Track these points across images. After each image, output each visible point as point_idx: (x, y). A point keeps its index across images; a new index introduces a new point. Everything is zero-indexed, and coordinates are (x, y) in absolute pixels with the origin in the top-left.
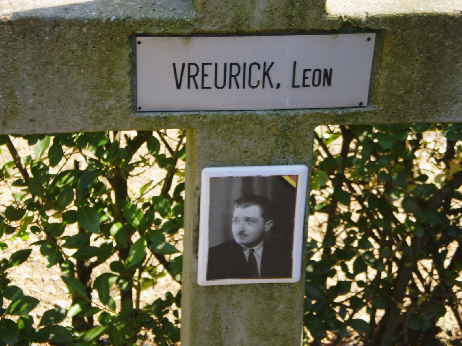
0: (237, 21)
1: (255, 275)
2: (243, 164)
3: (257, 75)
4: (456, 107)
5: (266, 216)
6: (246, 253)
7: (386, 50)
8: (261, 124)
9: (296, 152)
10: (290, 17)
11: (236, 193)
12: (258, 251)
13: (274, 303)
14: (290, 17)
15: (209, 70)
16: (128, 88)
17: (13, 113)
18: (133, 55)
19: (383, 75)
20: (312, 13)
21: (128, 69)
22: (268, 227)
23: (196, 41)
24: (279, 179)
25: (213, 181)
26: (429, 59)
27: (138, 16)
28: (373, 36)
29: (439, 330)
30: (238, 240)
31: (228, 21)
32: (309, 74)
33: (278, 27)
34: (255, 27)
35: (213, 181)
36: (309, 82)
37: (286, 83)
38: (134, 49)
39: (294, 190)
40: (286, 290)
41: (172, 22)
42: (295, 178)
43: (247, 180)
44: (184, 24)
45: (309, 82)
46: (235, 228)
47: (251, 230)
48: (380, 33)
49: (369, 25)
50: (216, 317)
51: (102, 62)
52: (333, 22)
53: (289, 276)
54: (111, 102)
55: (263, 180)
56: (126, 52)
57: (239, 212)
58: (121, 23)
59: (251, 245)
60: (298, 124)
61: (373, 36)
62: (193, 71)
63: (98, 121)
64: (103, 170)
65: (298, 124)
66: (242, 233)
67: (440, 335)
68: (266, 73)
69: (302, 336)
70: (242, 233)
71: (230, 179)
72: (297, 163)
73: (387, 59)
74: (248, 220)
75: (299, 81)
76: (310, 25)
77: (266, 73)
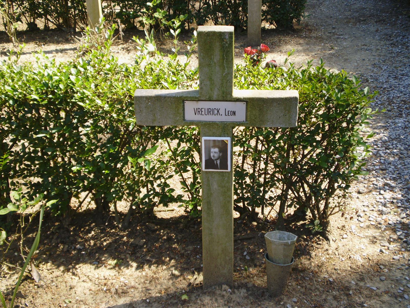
0: (210, 97)
1: (218, 169)
2: (213, 136)
3: (216, 112)
4: (269, 123)
5: (220, 151)
6: (215, 162)
7: (249, 106)
8: (217, 125)
9: (227, 134)
10: (223, 97)
11: (212, 144)
12: (218, 162)
13: (224, 177)
14: (223, 97)
15: (203, 110)
16: (182, 114)
17: (155, 120)
18: (184, 105)
19: (249, 113)
20: (229, 96)
21: (182, 109)
22: (221, 154)
23: (200, 102)
24: (223, 141)
25: (205, 141)
26: (260, 109)
27: (185, 96)
28: (245, 103)
29: (307, 215)
30: (213, 158)
31: (207, 97)
32: (229, 112)
33: (220, 99)
34: (214, 99)
35: (205, 141)
36: (229, 114)
37: (224, 114)
38: (184, 104)
39: (227, 144)
40: (227, 174)
41: (193, 97)
42: (227, 141)
43: (214, 141)
44: (196, 98)
45: (229, 114)
46: (212, 155)
47: (216, 155)
48: (247, 102)
49: (244, 100)
50: (208, 180)
51: (176, 107)
52: (234, 98)
53: (227, 169)
54: (178, 118)
55: (218, 141)
56: (182, 105)
57: (212, 150)
58: (181, 97)
59: (216, 160)
60: (228, 126)
61: (245, 103)
62: (199, 110)
63: (175, 123)
64: (304, 167)
65: (228, 126)
66: (214, 156)
67: (307, 217)
68: (218, 111)
69: (233, 191)
70: (214, 156)
71: (210, 140)
72: (228, 137)
73: (249, 109)
74: (215, 152)
75: (227, 114)
76: (228, 99)
77: (218, 111)
